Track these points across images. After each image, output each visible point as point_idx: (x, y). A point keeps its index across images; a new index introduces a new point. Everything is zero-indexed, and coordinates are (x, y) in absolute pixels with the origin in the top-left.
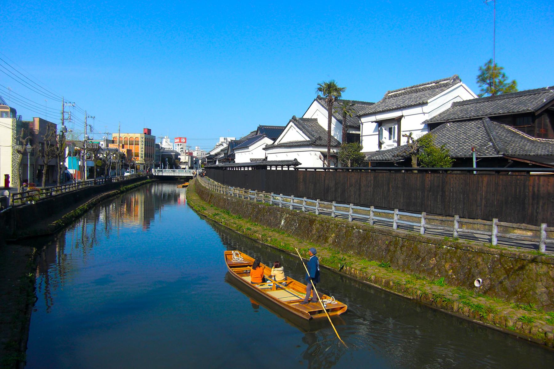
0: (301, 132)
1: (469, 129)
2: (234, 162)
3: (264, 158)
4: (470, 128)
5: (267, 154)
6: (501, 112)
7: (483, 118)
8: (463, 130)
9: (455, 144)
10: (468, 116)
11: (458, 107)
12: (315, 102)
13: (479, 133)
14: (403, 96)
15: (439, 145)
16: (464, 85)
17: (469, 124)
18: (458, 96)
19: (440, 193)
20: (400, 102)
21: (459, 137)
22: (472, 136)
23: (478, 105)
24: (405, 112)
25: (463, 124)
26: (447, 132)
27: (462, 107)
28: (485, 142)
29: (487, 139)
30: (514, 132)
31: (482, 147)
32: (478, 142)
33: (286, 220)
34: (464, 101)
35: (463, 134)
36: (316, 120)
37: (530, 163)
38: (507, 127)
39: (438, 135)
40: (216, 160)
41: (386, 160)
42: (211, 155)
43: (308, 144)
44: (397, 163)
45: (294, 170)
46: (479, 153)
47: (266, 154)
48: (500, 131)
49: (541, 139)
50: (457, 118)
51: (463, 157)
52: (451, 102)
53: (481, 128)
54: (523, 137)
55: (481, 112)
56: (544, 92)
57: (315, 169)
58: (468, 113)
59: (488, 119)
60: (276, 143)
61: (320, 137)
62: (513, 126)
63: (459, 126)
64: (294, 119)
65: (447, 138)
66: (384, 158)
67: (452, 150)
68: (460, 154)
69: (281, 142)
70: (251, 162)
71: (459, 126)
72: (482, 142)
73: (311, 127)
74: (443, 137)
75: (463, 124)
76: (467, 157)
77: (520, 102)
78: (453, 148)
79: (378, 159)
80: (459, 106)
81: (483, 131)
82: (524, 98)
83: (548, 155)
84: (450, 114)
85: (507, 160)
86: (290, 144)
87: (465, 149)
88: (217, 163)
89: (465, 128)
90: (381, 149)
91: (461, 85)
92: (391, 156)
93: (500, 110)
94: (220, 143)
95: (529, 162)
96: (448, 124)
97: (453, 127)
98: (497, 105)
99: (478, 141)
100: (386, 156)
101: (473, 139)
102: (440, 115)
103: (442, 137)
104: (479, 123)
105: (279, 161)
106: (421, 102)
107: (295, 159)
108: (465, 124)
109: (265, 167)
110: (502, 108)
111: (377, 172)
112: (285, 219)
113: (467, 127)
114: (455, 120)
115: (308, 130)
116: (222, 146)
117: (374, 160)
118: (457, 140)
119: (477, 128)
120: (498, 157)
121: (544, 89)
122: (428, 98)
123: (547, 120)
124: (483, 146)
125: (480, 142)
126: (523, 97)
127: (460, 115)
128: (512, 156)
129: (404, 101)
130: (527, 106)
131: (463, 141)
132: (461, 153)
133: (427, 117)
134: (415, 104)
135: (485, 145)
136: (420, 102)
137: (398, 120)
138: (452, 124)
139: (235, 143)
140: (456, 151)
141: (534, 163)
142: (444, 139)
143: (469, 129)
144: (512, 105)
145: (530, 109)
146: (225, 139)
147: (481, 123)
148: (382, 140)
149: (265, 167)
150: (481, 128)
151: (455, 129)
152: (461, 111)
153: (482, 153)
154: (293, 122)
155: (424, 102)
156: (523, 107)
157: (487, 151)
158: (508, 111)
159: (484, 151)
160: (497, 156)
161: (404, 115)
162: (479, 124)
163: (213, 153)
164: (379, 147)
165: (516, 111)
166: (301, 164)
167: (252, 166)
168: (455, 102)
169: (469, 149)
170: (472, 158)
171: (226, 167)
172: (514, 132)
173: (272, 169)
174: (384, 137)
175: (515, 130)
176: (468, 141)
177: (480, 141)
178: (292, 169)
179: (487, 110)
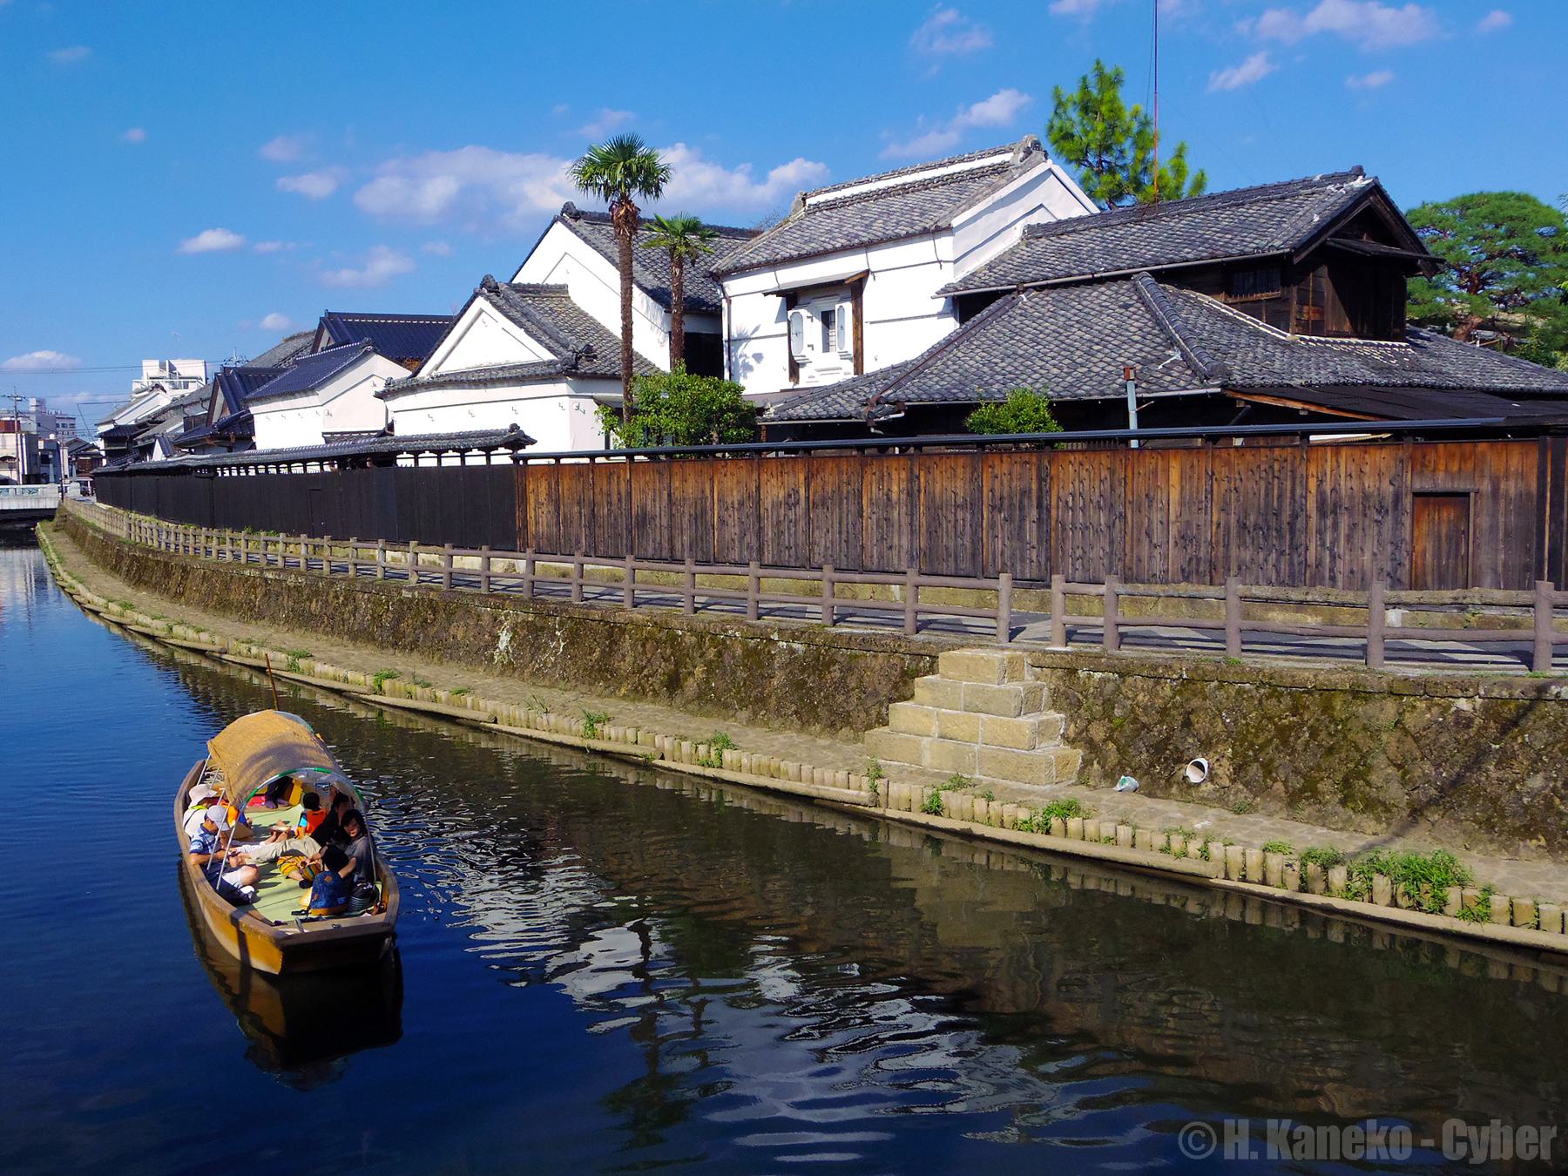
0: (520, 333)
1: (1093, 309)
2: (253, 446)
3: (381, 426)
4: (1098, 308)
5: (391, 415)
6: (1189, 256)
7: (1135, 276)
8: (1075, 315)
9: (1059, 357)
10: (1086, 270)
11: (1042, 240)
12: (559, 226)
13: (1130, 321)
14: (859, 206)
15: (1009, 364)
16: (1057, 169)
17: (1090, 294)
18: (1041, 206)
19: (1034, 514)
20: (854, 226)
21: (1067, 337)
22: (1107, 332)
23: (1109, 233)
24: (877, 259)
25: (1072, 296)
26: (1027, 322)
27: (1056, 243)
28: (1154, 348)
29: (1159, 340)
30: (1229, 316)
31: (1151, 366)
32: (1132, 350)
33: (515, 632)
34: (1059, 222)
35: (1077, 326)
36: (562, 290)
37: (1303, 409)
38: (1205, 299)
39: (999, 332)
40: (153, 445)
41: (840, 417)
42: (118, 428)
43: (550, 374)
44: (879, 425)
45: (511, 462)
46: (1144, 385)
47: (387, 410)
48: (1191, 313)
49: (1307, 337)
50: (1050, 275)
51: (1096, 397)
52: (1020, 226)
53: (1131, 306)
54: (1256, 334)
55: (1125, 257)
56: (1309, 191)
57: (558, 457)
58: (1082, 261)
59: (1150, 279)
60: (425, 373)
61: (589, 349)
62: (1223, 295)
63: (1060, 301)
64: (490, 289)
65: (1030, 339)
66: (832, 411)
67: (1056, 376)
68: (1087, 391)
69: (443, 370)
70: (327, 442)
71: (1060, 301)
72: (1147, 349)
73: (550, 315)
74: (1017, 338)
75: (1072, 296)
76: (1107, 397)
77: (1241, 222)
78: (1056, 371)
79: (811, 413)
80: (1047, 237)
81: (1142, 316)
82: (1251, 211)
83: (1335, 384)
84: (1022, 265)
85: (1234, 400)
86: (482, 376)
87: (1098, 374)
88: (158, 455)
89: (1080, 307)
90: (797, 383)
91: (1050, 171)
92: (855, 404)
93: (1186, 250)
94: (147, 382)
95: (1298, 406)
96: (1023, 296)
97: (1043, 306)
98: (1170, 232)
99: (1131, 346)
100: (837, 402)
101: (1116, 342)
102: (990, 267)
103: (1012, 339)
104: (1122, 291)
105: (449, 437)
106: (929, 224)
107: (514, 427)
108: (1078, 296)
109: (388, 458)
110: (1191, 244)
111: (930, 455)
112: (513, 630)
113: (1085, 303)
114: (1044, 282)
115: (544, 324)
116: (161, 392)
117: (800, 419)
118: (1063, 346)
119: (1120, 307)
120: (1206, 394)
121: (1307, 183)
122: (953, 214)
123: (1323, 281)
124: (1152, 362)
125: (1141, 350)
126: (1247, 206)
127: (1059, 267)
128: (1248, 390)
129: (867, 222)
130: (1266, 236)
131: (1085, 348)
132: (1086, 387)
133: (951, 276)
134: (911, 231)
135: (1159, 360)
136: (927, 226)
137: (853, 288)
138: (1034, 297)
139: (239, 376)
140: (1069, 379)
141: (1313, 408)
142: (1020, 344)
143: (1093, 309)
144: (1217, 232)
145: (1277, 243)
146: (162, 367)
147: (1128, 290)
148: (802, 354)
149: (388, 458)
150: (1131, 306)
151: (1049, 310)
152: (1060, 253)
153: (1155, 384)
154: (488, 298)
155: (939, 224)
156: (1256, 239)
157: (1169, 378)
158: (1210, 250)
159: (1161, 378)
160: (1204, 391)
161: (872, 270)
162: (1123, 295)
163: (127, 420)
164: (791, 376)
165: (1234, 251)
166: (533, 442)
167: (331, 459)
168: (1042, 223)
169: (1110, 372)
170: (1126, 399)
171: (212, 468)
172: (1226, 318)
173: (443, 465)
174: (807, 341)
175: (1232, 312)
176: (1099, 347)
177: (1139, 346)
178: (502, 458)
179: (1143, 251)
